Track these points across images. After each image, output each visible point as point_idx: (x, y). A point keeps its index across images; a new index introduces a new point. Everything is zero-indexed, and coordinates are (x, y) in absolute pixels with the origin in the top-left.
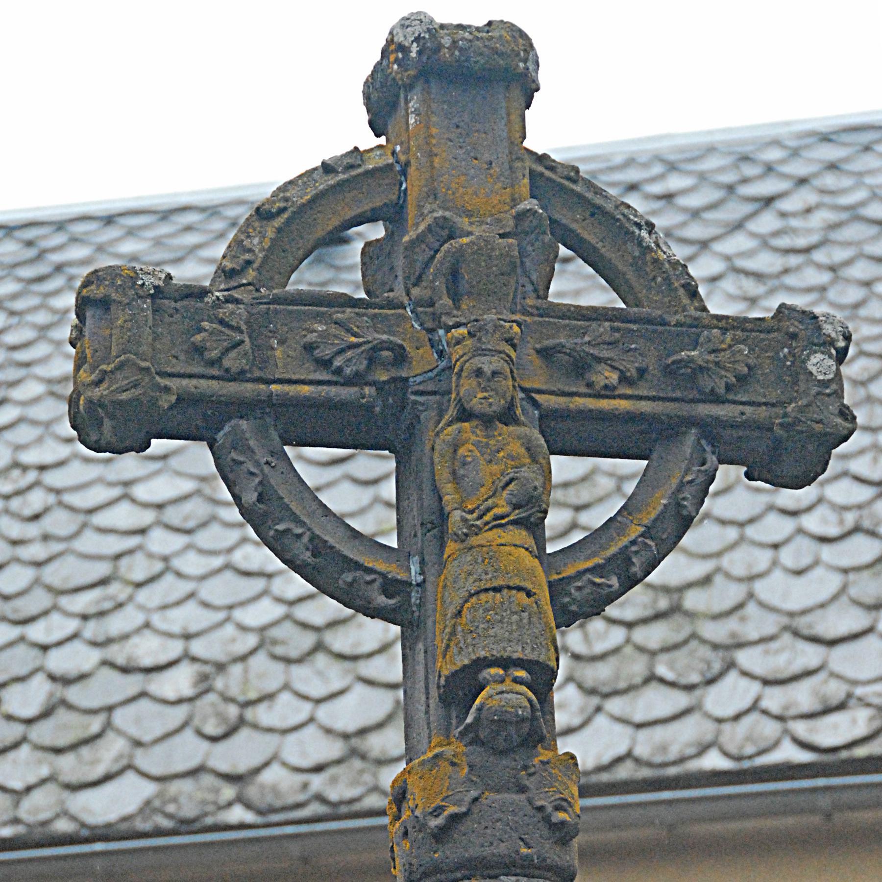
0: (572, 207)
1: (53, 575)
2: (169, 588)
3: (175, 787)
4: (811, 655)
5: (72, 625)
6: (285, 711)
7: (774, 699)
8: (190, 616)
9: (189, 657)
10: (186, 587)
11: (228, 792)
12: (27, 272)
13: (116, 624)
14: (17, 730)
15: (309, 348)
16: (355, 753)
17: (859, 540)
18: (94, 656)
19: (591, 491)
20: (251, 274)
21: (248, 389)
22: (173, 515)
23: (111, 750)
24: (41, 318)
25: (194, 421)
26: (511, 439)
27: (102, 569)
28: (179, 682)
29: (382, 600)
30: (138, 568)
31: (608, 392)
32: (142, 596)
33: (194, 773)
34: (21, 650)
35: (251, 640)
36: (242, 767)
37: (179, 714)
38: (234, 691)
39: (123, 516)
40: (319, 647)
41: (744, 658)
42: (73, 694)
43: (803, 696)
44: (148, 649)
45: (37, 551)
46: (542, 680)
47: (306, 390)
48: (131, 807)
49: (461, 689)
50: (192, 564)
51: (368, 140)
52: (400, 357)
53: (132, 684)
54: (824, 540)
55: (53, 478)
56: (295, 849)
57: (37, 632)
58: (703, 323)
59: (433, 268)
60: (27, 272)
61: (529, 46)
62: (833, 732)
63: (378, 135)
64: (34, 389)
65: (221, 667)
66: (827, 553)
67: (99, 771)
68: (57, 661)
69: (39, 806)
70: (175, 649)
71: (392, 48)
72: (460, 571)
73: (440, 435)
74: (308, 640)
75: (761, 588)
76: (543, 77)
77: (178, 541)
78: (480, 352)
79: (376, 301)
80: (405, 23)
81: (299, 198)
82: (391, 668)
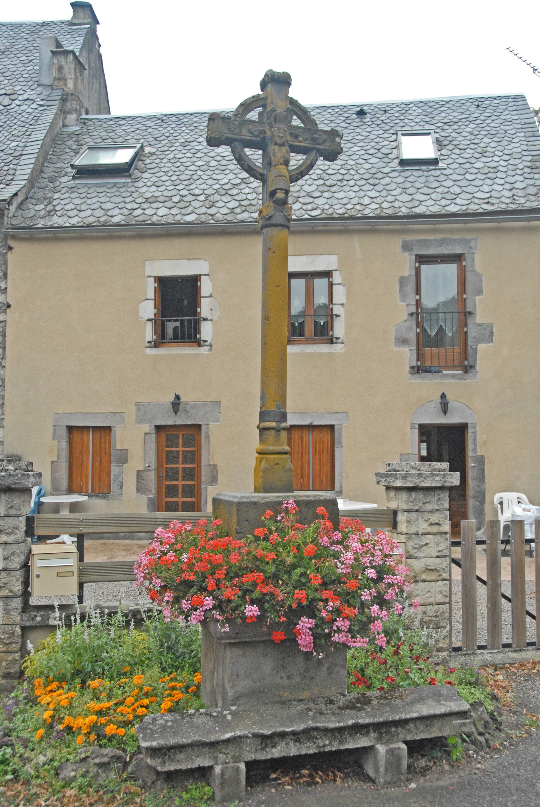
0: (296, 108)
1: (180, 177)
2: (201, 181)
3: (201, 216)
4: (311, 200)
5: (184, 187)
6: (220, 204)
7: (305, 207)
8: (204, 186)
9: (204, 193)
10: (204, 181)
11: (210, 217)
12: (177, 123)
13: (192, 187)
14: (174, 204)
15: (249, 130)
16: (232, 212)
17: (320, 180)
18: (188, 192)
19: (296, 160)
20: (239, 116)
21: (237, 137)
22: (202, 168)
23: (190, 209)
24: (179, 131)
25: (228, 142)
26: (285, 149)
27: (189, 177)
28: (202, 198)
29: (259, 177)
30: (196, 177)
31: (301, 142)
32: (196, 182)
33: (205, 214)
34: (175, 190)
35: (215, 191)
36: (213, 213)
37: (202, 203)
38: (212, 200)
39: (193, 168)
40: (227, 193)
41: (300, 200)
42: (184, 199)
43: (309, 207)
44: (197, 192)
45: (178, 173)
46: (287, 192)
47: (248, 138)
48: (194, 219)
49: (273, 194)
50: (205, 177)
51: (261, 93)
52: (265, 132)
53: (194, 198)
54: (314, 180)
55: (181, 160)
56: (221, 228)
57: (178, 187)
58: (317, 131)
59: (270, 117)
60: (177, 123)
61: (290, 77)
62: (314, 213)
63: (262, 90)
64: (178, 144)
65: (209, 196)
66: (315, 182)
67: (188, 212)
68: (182, 193)
69: (178, 218)
70: (201, 192)
71: (266, 75)
72: (274, 172)
73: (272, 148)
74: (224, 192)
75: (304, 188)
76: (292, 83)
77: (203, 173)
78: (279, 132)
79: (261, 121)
80: (269, 71)
81: (248, 102)
82: (260, 190)
